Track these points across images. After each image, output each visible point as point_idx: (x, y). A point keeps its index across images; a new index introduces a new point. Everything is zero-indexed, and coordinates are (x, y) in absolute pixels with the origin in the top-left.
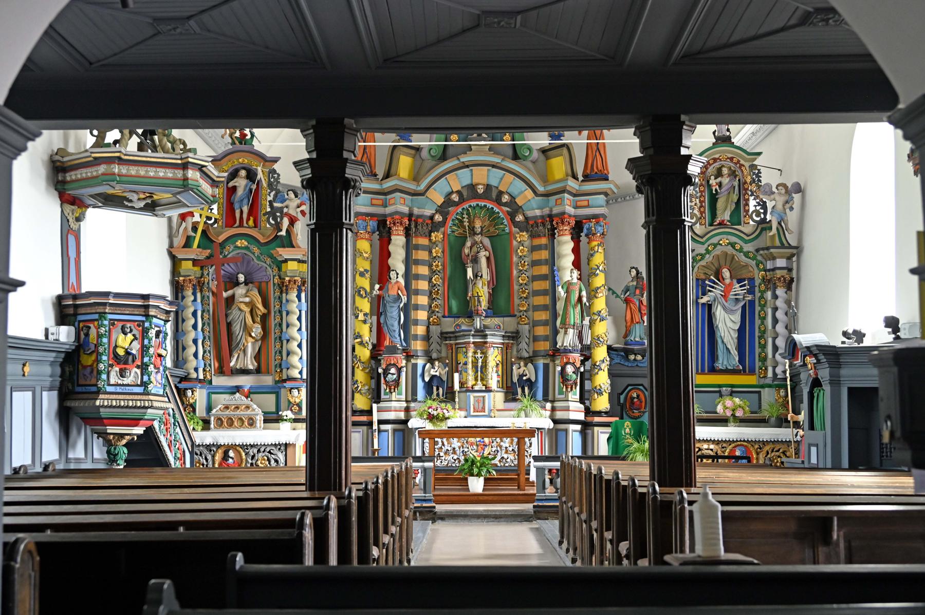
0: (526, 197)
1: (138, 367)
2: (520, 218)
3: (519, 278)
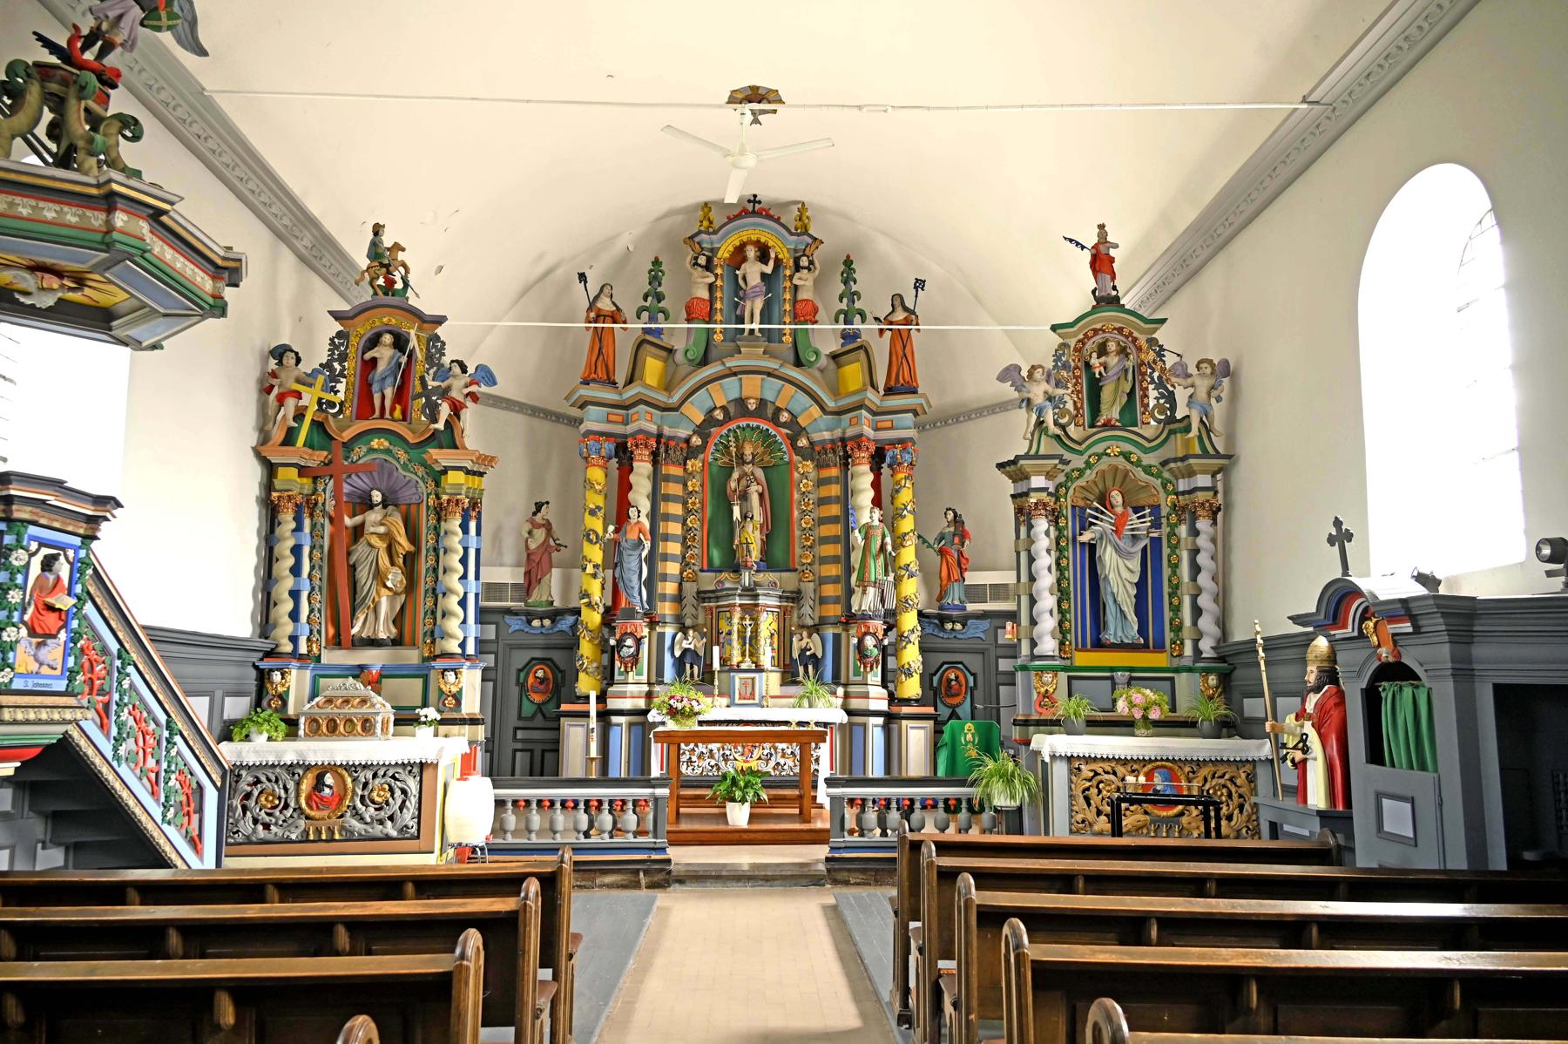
0: (811, 415)
2: (803, 442)
3: (801, 520)
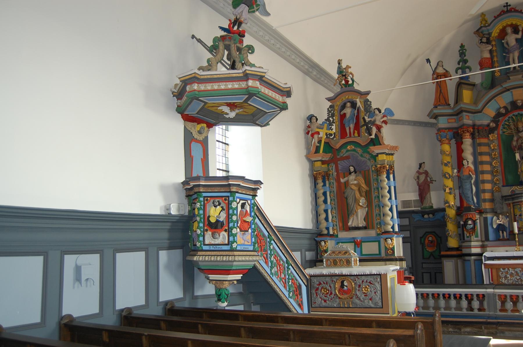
1: (226, 231)
